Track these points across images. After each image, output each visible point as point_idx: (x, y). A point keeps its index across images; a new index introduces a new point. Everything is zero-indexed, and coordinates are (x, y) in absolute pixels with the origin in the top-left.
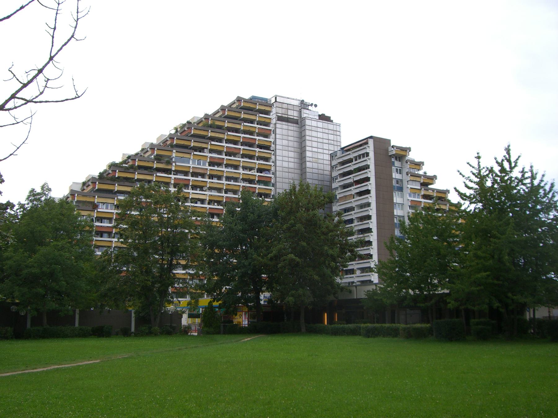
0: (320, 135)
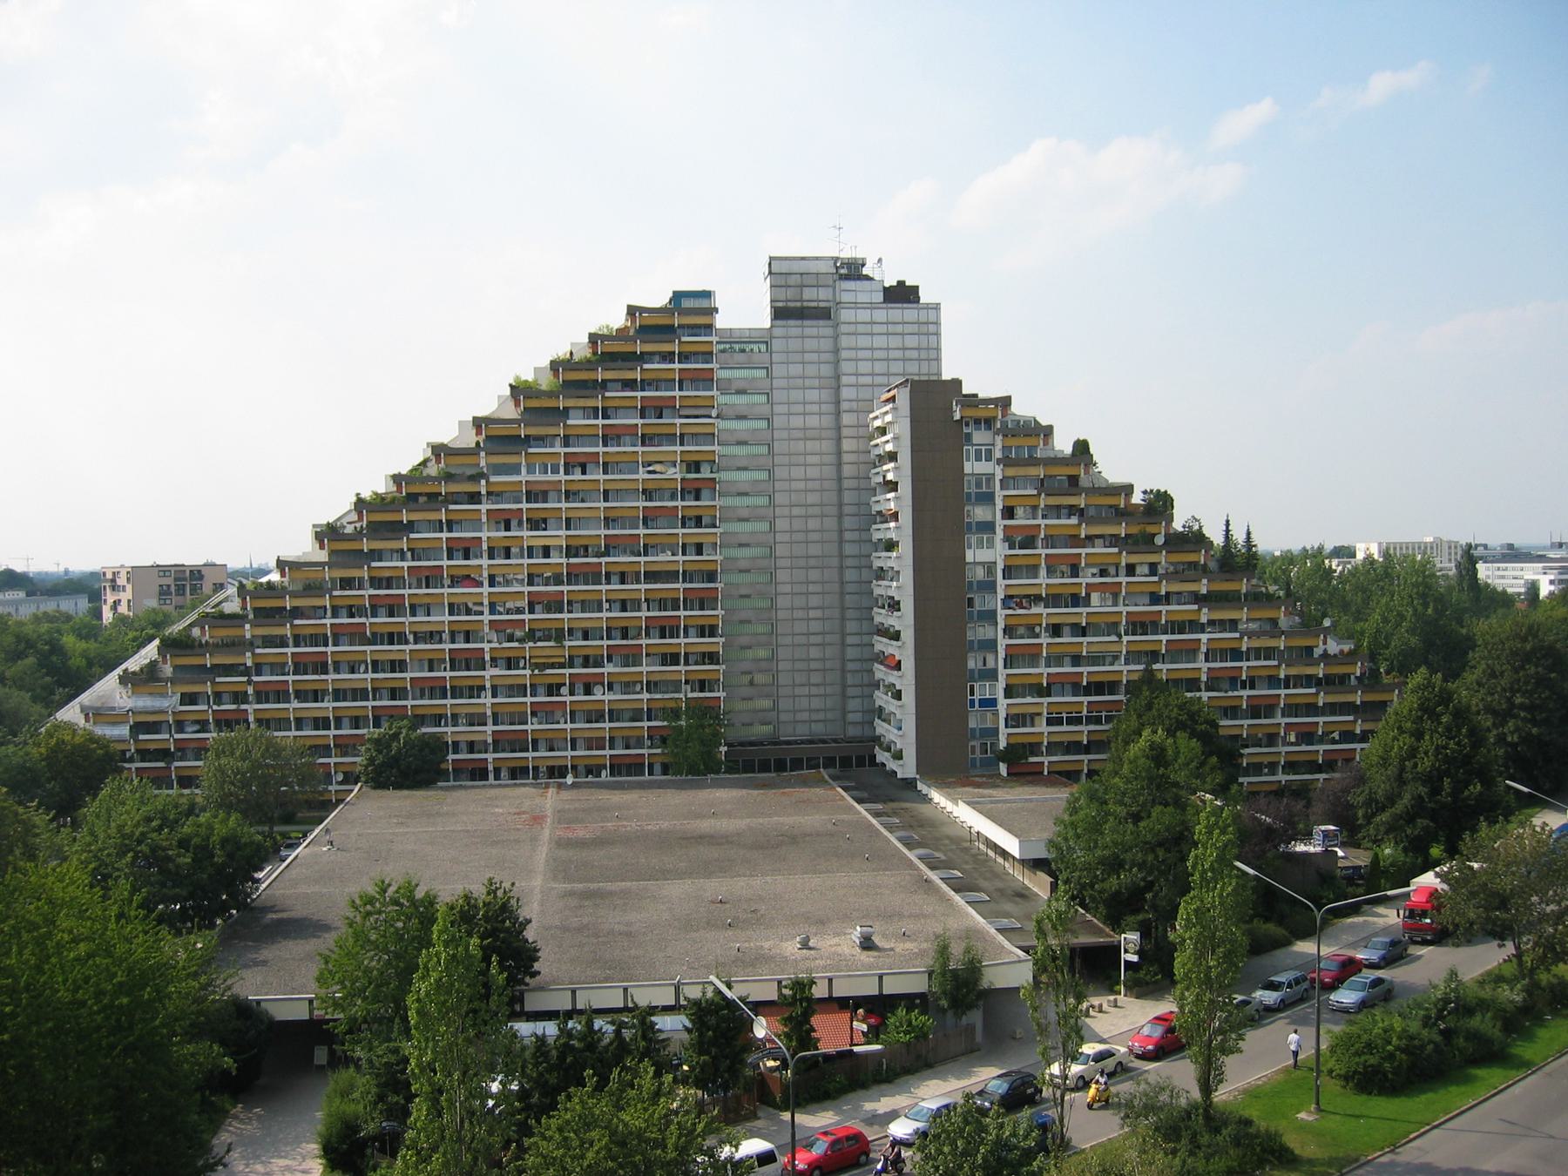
0: (880, 341)
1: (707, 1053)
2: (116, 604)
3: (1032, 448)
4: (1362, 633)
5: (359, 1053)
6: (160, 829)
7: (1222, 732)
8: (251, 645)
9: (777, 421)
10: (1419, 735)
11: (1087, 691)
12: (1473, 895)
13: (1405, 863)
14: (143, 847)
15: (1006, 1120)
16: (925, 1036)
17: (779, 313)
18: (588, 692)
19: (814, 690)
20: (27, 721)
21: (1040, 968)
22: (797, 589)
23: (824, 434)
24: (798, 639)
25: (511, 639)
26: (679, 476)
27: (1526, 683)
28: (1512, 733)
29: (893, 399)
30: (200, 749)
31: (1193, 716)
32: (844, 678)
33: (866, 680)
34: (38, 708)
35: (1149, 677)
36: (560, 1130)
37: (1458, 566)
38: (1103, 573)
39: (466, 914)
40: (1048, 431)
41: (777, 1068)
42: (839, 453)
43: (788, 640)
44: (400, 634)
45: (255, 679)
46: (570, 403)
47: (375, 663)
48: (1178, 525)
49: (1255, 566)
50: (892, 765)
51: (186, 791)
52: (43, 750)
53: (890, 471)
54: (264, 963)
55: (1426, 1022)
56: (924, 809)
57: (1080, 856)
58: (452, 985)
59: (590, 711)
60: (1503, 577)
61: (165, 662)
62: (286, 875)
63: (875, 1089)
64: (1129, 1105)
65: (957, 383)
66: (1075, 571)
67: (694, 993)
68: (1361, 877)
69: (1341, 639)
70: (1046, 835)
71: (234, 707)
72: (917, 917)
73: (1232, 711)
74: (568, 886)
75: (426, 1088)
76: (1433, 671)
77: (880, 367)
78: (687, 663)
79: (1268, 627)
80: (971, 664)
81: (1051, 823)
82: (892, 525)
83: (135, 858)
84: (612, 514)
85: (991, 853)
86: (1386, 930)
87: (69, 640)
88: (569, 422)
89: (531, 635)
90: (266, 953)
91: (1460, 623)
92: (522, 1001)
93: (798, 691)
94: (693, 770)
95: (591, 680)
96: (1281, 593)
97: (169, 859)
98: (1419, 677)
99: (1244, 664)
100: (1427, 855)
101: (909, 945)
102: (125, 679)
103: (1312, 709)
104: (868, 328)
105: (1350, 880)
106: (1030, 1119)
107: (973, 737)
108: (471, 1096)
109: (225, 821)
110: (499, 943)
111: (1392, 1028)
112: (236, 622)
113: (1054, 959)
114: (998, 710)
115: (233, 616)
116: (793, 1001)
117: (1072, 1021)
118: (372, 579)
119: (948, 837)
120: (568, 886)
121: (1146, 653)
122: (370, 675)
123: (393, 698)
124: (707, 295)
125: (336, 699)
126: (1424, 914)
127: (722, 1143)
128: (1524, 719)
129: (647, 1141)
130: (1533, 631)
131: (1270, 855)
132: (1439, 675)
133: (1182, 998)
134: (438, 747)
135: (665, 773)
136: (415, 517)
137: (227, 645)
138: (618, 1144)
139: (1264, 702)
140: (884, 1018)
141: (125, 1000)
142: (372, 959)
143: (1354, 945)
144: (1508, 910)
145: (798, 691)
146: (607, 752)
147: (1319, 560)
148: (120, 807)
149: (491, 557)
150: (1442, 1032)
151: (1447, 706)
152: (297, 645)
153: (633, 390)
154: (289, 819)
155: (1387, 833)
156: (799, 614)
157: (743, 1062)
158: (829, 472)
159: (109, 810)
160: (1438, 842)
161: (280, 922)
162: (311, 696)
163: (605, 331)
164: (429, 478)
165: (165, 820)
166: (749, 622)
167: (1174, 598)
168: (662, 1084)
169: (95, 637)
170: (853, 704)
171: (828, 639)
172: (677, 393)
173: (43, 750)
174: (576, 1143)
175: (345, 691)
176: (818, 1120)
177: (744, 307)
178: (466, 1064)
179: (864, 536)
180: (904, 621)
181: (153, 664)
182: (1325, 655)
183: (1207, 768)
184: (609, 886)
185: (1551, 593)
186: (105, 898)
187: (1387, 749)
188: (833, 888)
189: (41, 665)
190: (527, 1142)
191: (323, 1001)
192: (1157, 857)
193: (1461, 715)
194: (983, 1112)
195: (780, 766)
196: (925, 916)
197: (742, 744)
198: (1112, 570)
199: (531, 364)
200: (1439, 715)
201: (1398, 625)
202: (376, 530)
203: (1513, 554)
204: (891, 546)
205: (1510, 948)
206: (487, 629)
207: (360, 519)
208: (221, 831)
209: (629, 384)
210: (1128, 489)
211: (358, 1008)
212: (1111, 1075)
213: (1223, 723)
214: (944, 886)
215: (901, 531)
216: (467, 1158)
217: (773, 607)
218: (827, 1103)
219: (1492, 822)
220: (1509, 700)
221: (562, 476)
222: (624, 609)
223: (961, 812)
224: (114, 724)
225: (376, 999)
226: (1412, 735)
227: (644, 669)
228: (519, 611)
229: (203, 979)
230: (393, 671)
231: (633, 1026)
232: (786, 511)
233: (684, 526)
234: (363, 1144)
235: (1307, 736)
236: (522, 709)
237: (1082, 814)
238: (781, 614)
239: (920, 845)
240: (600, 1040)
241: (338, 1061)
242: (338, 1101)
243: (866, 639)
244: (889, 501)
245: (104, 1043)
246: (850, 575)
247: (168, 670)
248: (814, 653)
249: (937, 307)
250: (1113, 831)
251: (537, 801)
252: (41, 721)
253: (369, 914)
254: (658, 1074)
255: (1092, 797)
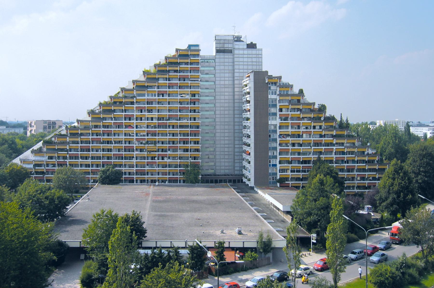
0: (246, 60)
1: (194, 260)
2: (31, 131)
3: (287, 91)
4: (378, 148)
5: (93, 256)
6: (40, 194)
7: (339, 176)
8: (69, 143)
9: (217, 82)
10: (394, 179)
11: (302, 163)
12: (409, 230)
13: (390, 218)
14: (35, 199)
15: (279, 284)
16: (256, 259)
17: (218, 51)
18: (163, 159)
19: (226, 160)
20: (4, 162)
21: (288, 243)
22: (222, 131)
23: (230, 86)
24: (222, 146)
25: (141, 143)
26: (189, 98)
27: (424, 164)
28: (420, 179)
29: (249, 76)
30: (53, 172)
31: (331, 171)
32: (234, 157)
33: (240, 158)
34: (8, 159)
35: (319, 159)
36: (151, 278)
37: (405, 128)
38: (307, 128)
39: (126, 220)
40: (292, 87)
41: (214, 265)
42: (234, 92)
43: (219, 146)
44: (110, 141)
45: (69, 153)
46: (159, 76)
47: (103, 149)
48: (327, 115)
49: (349, 127)
50: (247, 182)
51: (48, 183)
52: (8, 171)
53: (248, 97)
54: (68, 231)
55: (397, 269)
56: (256, 195)
57: (300, 211)
58: (122, 239)
59: (163, 165)
60: (417, 131)
61: (44, 147)
62: (76, 207)
63: (242, 273)
64: (314, 284)
65: (267, 72)
66: (299, 127)
67: (191, 244)
68: (378, 222)
69: (372, 149)
70: (290, 205)
71: (63, 160)
72: (254, 226)
73: (342, 170)
74: (156, 213)
75: (113, 266)
76: (398, 160)
77: (245, 67)
78: (190, 152)
79: (352, 145)
80: (270, 154)
81: (292, 201)
82: (248, 113)
83: (32, 201)
84: (170, 109)
85: (275, 209)
86: (385, 239)
87: (17, 141)
88: (159, 82)
89: (147, 143)
90: (69, 228)
91: (405, 145)
92: (141, 244)
93: (221, 160)
94: (192, 182)
95: (164, 156)
96: (356, 135)
97: (42, 202)
98: (394, 161)
99: (346, 156)
100: (396, 217)
101: (251, 234)
102: (32, 152)
103: (364, 170)
104: (242, 56)
105: (375, 223)
106: (286, 285)
107: (270, 175)
108: (126, 268)
109: (59, 192)
110: (136, 228)
111: (388, 270)
112: (65, 137)
113: (292, 240)
114: (277, 169)
115: (64, 135)
116: (219, 247)
117: (298, 258)
118: (103, 126)
119: (263, 204)
120: (156, 213)
121: (318, 152)
122: (102, 153)
123: (108, 159)
124: (198, 46)
125: (92, 159)
126: (396, 235)
127: (198, 284)
128: (423, 175)
129: (176, 282)
130: (425, 148)
131: (353, 214)
132: (400, 161)
133: (328, 254)
134: (120, 173)
135: (184, 183)
136: (116, 108)
137: (62, 143)
138: (168, 283)
139: (351, 168)
140: (244, 254)
141: (26, 240)
142: (99, 231)
143: (376, 243)
144: (419, 236)
145: (221, 160)
146: (168, 176)
147: (366, 125)
148: (29, 187)
149: (137, 120)
150: (402, 273)
151: (402, 171)
152: (81, 144)
153: (177, 73)
154: (77, 192)
155: (385, 209)
156: (222, 138)
157: (204, 263)
158: (231, 97)
159: (26, 188)
160: (400, 213)
161: (73, 220)
162: (85, 158)
163: (169, 56)
164: (120, 97)
165: (42, 191)
166: (208, 140)
167: (326, 136)
168: (181, 268)
169: (25, 140)
170: (237, 165)
171: (230, 146)
172: (189, 74)
173: (8, 171)
174: (155, 282)
175: (95, 157)
176: (225, 280)
177: (208, 50)
178: (125, 260)
179: (241, 116)
180: (251, 141)
181: (41, 148)
182: (368, 154)
183: (335, 187)
184: (168, 214)
185: (431, 137)
186: (23, 212)
187: (385, 183)
188: (230, 217)
189: (9, 147)
190: (141, 281)
191: (84, 242)
192: (321, 212)
193: (405, 173)
194: (273, 281)
195: (216, 182)
196: (256, 226)
197: (205, 175)
198: (309, 128)
199: (149, 66)
200: (400, 173)
201: (388, 145)
202: (105, 111)
203: (420, 125)
204: (248, 119)
205: (420, 248)
206: (135, 141)
207: (100, 108)
208: (57, 195)
209: (176, 71)
210: (314, 104)
211: (94, 244)
212: (308, 275)
213: (340, 173)
214: (261, 218)
215: (251, 115)
216: (124, 285)
217: (215, 136)
218: (228, 275)
219: (415, 207)
220: (419, 169)
221: (157, 97)
222: (173, 136)
223: (266, 196)
224: (29, 164)
225: (99, 242)
226: (392, 179)
227: (179, 153)
228: (144, 136)
229: (49, 235)
230: (108, 152)
231: (173, 252)
232: (219, 109)
233: (190, 112)
234: (93, 280)
235: (363, 178)
236: (144, 163)
237: (300, 199)
238: (217, 138)
239: (255, 206)
240: (163, 255)
241: (87, 258)
242: (86, 269)
243: (241, 146)
244: (247, 106)
245: (18, 252)
246: (236, 127)
247: (45, 149)
248: (226, 149)
249: (261, 50)
250: (309, 204)
251: (148, 189)
252: (8, 163)
253: (99, 219)
254: (180, 265)
255: (303, 194)
